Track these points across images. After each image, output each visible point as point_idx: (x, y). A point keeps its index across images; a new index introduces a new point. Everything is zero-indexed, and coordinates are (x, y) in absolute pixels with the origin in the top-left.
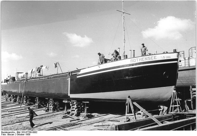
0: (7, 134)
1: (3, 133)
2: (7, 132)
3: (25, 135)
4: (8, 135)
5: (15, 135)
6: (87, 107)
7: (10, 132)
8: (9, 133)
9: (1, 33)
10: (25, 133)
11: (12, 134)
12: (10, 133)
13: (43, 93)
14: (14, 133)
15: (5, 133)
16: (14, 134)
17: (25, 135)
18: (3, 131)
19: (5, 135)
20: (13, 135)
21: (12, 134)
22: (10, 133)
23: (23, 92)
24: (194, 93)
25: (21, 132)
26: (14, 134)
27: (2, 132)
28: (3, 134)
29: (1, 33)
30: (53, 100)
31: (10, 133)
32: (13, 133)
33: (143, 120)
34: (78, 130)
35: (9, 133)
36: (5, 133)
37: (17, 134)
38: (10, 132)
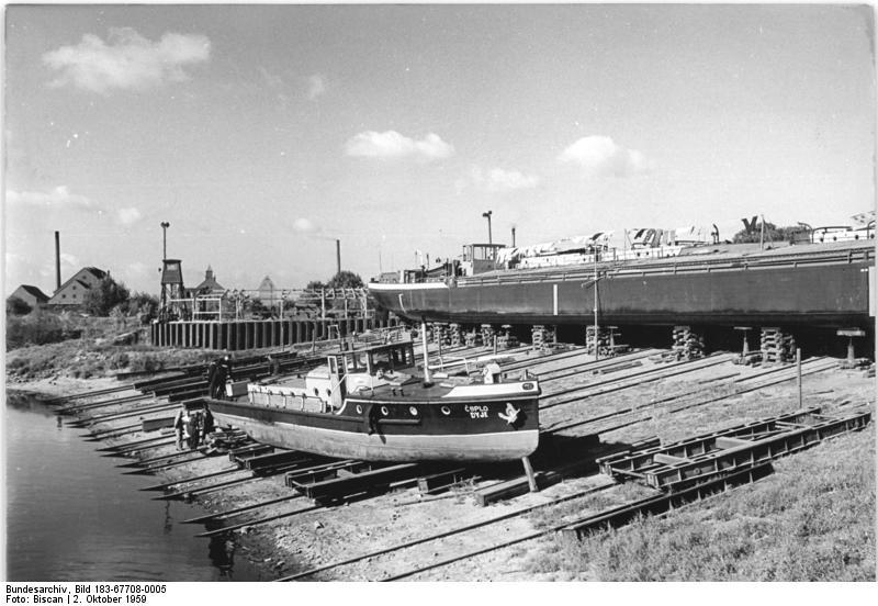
0: (30, 596)
1: (11, 593)
2: (31, 590)
3: (124, 600)
4: (36, 599)
5: (65, 599)
6: (505, 418)
7: (43, 590)
8: (38, 594)
9: (4, 229)
10: (714, 548)
11: (52, 595)
12: (46, 595)
13: (621, 310)
14: (61, 595)
15: (21, 595)
16: (64, 596)
17: (124, 600)
18: (15, 585)
19: (23, 600)
20: (56, 600)
21: (52, 595)
22: (43, 595)
23: (595, 310)
24: (870, 254)
25: (93, 589)
26: (64, 596)
27: (8, 589)
28: (16, 595)
29: (4, 229)
30: (780, 332)
31: (46, 595)
32: (59, 591)
33: (634, 504)
34: (698, 560)
35: (38, 594)
36: (21, 595)
37: (89, 599)
38: (43, 590)
